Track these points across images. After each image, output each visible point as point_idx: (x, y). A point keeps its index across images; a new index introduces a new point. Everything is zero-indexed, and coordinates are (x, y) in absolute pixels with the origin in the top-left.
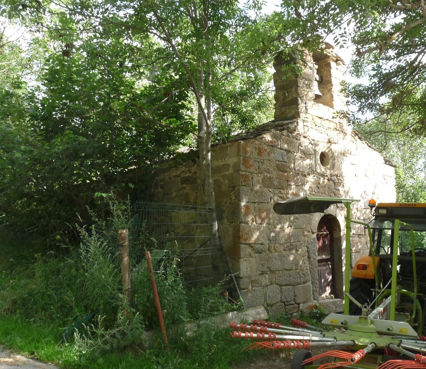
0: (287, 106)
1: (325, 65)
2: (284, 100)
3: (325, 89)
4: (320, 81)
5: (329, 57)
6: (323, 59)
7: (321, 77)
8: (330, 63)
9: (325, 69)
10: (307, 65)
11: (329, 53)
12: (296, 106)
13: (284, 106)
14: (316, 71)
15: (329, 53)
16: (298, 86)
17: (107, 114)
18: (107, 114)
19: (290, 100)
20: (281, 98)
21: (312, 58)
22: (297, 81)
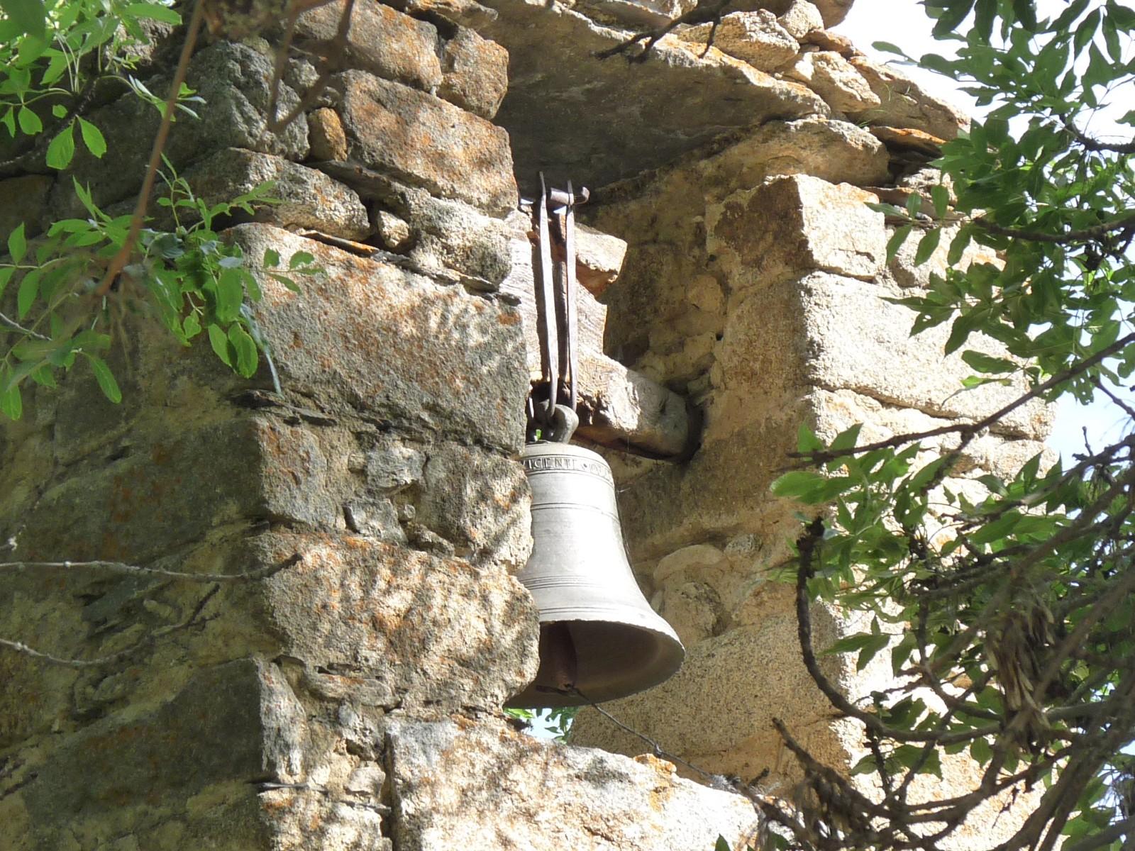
0: (122, 796)
1: (726, 227)
2: (96, 712)
3: (740, 547)
4: (670, 435)
5: (776, 113)
6: (710, 148)
7: (682, 398)
8: (788, 191)
9: (737, 274)
10: (425, 231)
11: (782, 64)
12: (233, 790)
13: (83, 803)
14: (587, 313)
15: (782, 64)
16: (264, 520)
17: (758, 504)
18: (758, 504)
19: (169, 711)
20: (59, 682)
21: (493, 139)
22: (248, 451)
